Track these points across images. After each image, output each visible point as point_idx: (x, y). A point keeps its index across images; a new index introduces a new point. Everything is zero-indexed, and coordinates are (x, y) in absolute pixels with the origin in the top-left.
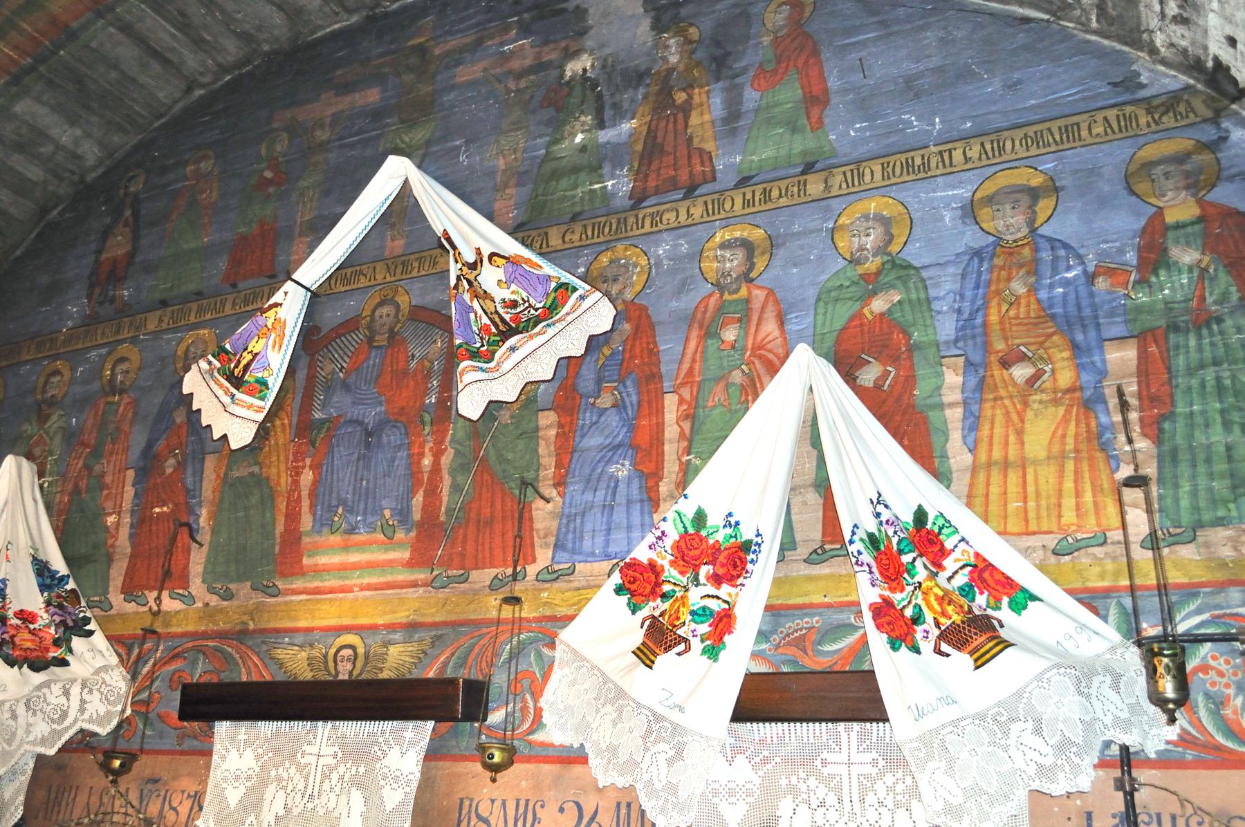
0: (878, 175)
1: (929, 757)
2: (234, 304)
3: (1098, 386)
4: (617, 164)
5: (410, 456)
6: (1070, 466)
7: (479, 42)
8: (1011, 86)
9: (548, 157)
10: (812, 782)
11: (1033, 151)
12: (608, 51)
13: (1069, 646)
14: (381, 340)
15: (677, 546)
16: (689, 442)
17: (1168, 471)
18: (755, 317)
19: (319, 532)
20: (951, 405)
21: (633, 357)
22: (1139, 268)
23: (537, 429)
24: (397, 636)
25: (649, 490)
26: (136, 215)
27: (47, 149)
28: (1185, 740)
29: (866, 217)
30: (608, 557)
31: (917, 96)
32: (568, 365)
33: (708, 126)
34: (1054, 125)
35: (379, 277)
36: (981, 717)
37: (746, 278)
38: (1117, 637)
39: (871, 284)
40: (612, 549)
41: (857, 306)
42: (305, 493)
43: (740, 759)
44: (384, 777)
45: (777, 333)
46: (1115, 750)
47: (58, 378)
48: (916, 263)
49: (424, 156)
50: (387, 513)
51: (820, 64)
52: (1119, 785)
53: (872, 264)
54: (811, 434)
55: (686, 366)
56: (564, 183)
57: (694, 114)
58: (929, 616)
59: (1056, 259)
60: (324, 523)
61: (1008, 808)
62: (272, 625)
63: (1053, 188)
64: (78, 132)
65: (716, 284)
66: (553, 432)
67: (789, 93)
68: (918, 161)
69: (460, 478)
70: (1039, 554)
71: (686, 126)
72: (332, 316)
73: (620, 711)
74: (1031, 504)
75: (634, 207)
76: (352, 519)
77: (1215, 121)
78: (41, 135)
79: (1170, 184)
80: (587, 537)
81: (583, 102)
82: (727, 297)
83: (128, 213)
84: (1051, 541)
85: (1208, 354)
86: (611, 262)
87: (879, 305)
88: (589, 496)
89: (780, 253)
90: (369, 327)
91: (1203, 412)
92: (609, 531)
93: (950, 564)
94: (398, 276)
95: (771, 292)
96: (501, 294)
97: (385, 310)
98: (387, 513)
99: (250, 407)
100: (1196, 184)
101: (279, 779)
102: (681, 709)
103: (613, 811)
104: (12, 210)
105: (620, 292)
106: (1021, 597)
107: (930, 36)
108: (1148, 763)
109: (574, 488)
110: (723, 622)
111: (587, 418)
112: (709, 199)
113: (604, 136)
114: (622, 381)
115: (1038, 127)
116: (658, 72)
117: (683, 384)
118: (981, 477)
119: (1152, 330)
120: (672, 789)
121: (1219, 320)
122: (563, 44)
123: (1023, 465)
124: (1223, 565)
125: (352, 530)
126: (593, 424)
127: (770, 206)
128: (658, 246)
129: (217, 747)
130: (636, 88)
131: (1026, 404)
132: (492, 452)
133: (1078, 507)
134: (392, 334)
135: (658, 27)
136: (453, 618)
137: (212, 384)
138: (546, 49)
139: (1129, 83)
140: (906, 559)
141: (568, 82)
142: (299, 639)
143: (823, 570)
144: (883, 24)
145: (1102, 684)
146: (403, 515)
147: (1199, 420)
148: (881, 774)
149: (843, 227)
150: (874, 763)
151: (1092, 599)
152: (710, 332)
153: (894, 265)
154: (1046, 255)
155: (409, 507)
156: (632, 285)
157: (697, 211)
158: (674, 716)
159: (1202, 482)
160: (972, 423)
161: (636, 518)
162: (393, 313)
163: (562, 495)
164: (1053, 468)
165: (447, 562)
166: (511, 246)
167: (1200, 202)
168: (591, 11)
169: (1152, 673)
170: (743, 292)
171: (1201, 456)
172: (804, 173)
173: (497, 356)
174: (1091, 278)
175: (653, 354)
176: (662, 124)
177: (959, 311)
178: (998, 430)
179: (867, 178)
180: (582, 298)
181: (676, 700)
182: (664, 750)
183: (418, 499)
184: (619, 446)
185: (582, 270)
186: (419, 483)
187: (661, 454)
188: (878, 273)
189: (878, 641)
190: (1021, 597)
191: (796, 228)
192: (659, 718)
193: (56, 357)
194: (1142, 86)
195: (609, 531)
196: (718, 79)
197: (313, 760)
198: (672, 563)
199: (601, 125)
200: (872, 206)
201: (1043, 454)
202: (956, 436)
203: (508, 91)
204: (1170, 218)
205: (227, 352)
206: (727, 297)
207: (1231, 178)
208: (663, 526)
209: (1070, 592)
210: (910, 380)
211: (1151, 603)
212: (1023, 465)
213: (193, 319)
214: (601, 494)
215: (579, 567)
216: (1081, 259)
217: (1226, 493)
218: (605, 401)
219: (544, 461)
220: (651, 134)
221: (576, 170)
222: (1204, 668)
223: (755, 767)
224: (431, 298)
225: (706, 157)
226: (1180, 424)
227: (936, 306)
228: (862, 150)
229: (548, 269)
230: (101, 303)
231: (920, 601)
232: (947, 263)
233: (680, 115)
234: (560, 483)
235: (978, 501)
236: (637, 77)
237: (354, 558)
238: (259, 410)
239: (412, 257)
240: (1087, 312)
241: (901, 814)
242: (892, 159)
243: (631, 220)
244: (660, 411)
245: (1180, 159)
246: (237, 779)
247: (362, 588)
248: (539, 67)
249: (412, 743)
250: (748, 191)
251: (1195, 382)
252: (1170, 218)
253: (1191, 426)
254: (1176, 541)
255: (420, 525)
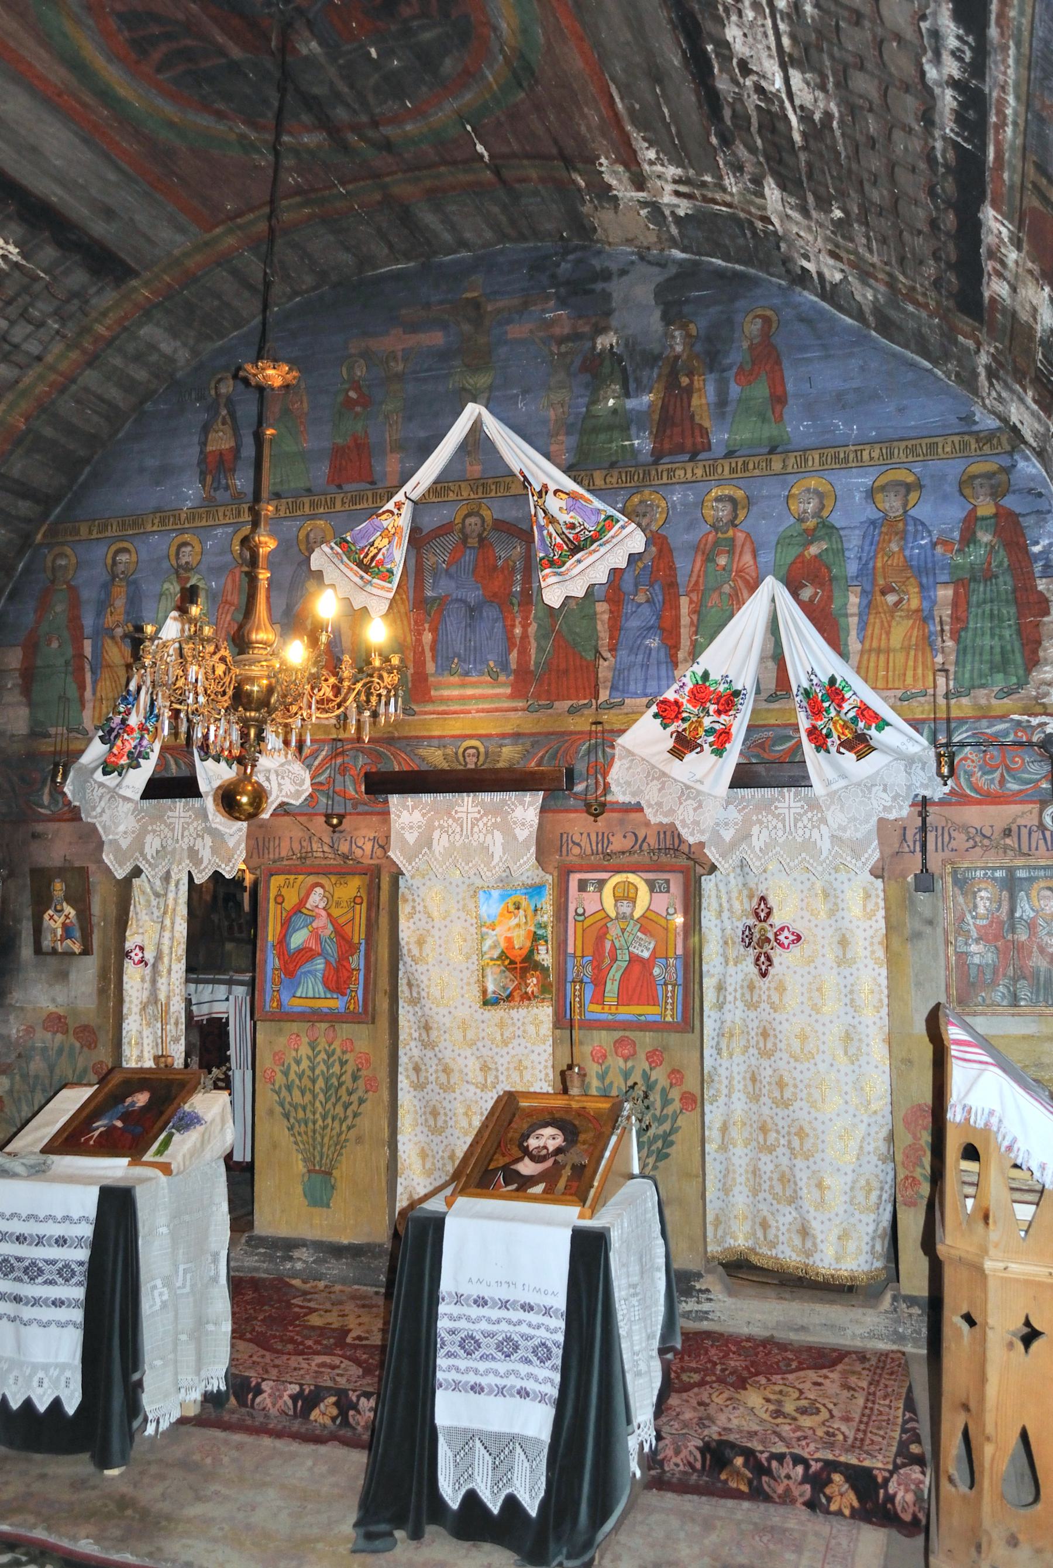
0: (817, 461)
1: (832, 802)
2: (343, 503)
3: (931, 610)
4: (641, 428)
5: (505, 626)
6: (912, 653)
7: (526, 305)
8: (901, 410)
9: (588, 415)
10: (770, 817)
11: (910, 459)
12: (630, 332)
13: (903, 748)
14: (473, 542)
15: (692, 691)
16: (697, 627)
17: (961, 658)
18: (738, 550)
19: (442, 675)
20: (852, 615)
21: (658, 570)
22: (960, 542)
23: (595, 614)
24: (507, 741)
25: (671, 656)
26: (232, 414)
27: (154, 358)
28: (952, 792)
29: (808, 490)
30: (646, 695)
31: (844, 407)
32: (615, 573)
33: (705, 408)
34: (924, 441)
35: (465, 494)
36: (859, 784)
37: (733, 523)
38: (926, 743)
39: (810, 536)
40: (649, 691)
41: (801, 549)
42: (427, 649)
43: (731, 807)
44: (515, 823)
45: (751, 562)
46: (920, 798)
47: (189, 548)
48: (837, 525)
49: (489, 399)
50: (492, 664)
51: (781, 370)
52: (920, 814)
53: (811, 523)
54: (773, 626)
55: (694, 579)
56: (602, 437)
57: (695, 396)
58: (835, 734)
59: (916, 531)
60: (445, 667)
61: (868, 826)
62: (413, 734)
63: (919, 486)
64: (179, 344)
65: (713, 526)
66: (606, 617)
67: (761, 390)
68: (842, 455)
69: (543, 643)
70: (892, 700)
71: (689, 406)
72: (431, 521)
73: (664, 783)
74: (890, 673)
75: (656, 462)
76: (466, 667)
77: (1011, 454)
78: (153, 347)
79: (982, 491)
80: (632, 683)
81: (612, 373)
82: (720, 535)
83: (224, 412)
84: (899, 693)
85: (988, 596)
86: (641, 502)
87: (814, 550)
88: (632, 658)
89: (754, 509)
90: (462, 530)
91: (982, 628)
92: (646, 680)
93: (846, 706)
94: (480, 495)
95: (748, 535)
96: (564, 518)
97: (472, 520)
98: (492, 664)
99: (383, 588)
100: (997, 493)
101: (441, 827)
102: (702, 783)
103: (656, 837)
104: (121, 405)
105: (648, 525)
106: (882, 724)
107: (854, 363)
108: (935, 804)
109: (623, 653)
110: (723, 736)
111: (629, 608)
112: (707, 463)
113: (631, 404)
114: (651, 585)
115: (914, 442)
116: (667, 357)
117: (692, 591)
118: (866, 657)
119: (962, 580)
120: (696, 823)
121: (996, 577)
122: (594, 320)
123: (888, 651)
124: (981, 708)
125: (467, 674)
126: (633, 613)
127: (747, 474)
128: (673, 494)
129: (392, 809)
130: (652, 368)
131: (893, 617)
132: (564, 627)
133: (914, 676)
134: (481, 540)
135: (667, 319)
136: (545, 730)
137: (342, 567)
138: (581, 322)
139: (968, 419)
140: (826, 705)
141: (600, 354)
142: (435, 742)
143: (776, 706)
144: (824, 347)
145: (917, 767)
146: (504, 666)
147: (979, 632)
148: (806, 812)
149: (794, 495)
150: (802, 807)
151: (916, 724)
152: (709, 558)
153: (824, 525)
154: (911, 528)
155: (507, 662)
156: (656, 520)
157: (699, 472)
158: (698, 786)
159: (976, 665)
160: (863, 626)
161: (663, 673)
162: (479, 522)
163: (614, 657)
164: (904, 654)
165: (538, 696)
166: (570, 485)
167: (997, 505)
168: (615, 295)
169: (939, 763)
170: (730, 533)
171: (978, 651)
172: (771, 452)
173: (568, 565)
174: (934, 545)
175: (672, 568)
176: (673, 400)
177: (860, 558)
178: (877, 631)
179: (810, 463)
180: (623, 527)
181: (697, 777)
182: (691, 804)
183: (514, 655)
184: (651, 628)
185: (620, 505)
186: (514, 645)
187: (679, 635)
188: (814, 530)
189: (808, 747)
190: (882, 724)
191: (765, 492)
192: (688, 787)
193: (183, 531)
194: (975, 423)
195: (646, 680)
196: (711, 371)
197: (464, 815)
198: (689, 701)
199: (627, 395)
200: (813, 483)
201: (899, 646)
202: (853, 633)
203: (552, 354)
204: (980, 513)
205: (347, 542)
206: (720, 535)
207: (1014, 492)
208: (684, 680)
209: (906, 720)
210: (830, 599)
211: (943, 726)
212: (888, 651)
213: (307, 511)
214: (640, 657)
215: (627, 701)
216: (929, 532)
217: (987, 671)
218: (641, 598)
219: (602, 635)
220: (664, 408)
221: (610, 428)
222: (965, 759)
223: (739, 811)
224: (511, 514)
225: (704, 432)
226: (970, 634)
227: (847, 554)
228: (809, 442)
229: (597, 504)
230: (216, 489)
231: (831, 726)
232: (855, 527)
233: (685, 396)
234: (613, 649)
235: (863, 671)
236: (652, 359)
237: (470, 692)
238: (389, 590)
239: (490, 481)
240: (930, 565)
241: (816, 830)
242: (826, 451)
243: (653, 472)
244: (678, 607)
245: (989, 476)
246: (411, 828)
247: (478, 711)
248: (575, 336)
249: (531, 804)
250: (733, 461)
251: (980, 611)
252: (980, 513)
253: (975, 635)
254: (959, 695)
255: (516, 672)
